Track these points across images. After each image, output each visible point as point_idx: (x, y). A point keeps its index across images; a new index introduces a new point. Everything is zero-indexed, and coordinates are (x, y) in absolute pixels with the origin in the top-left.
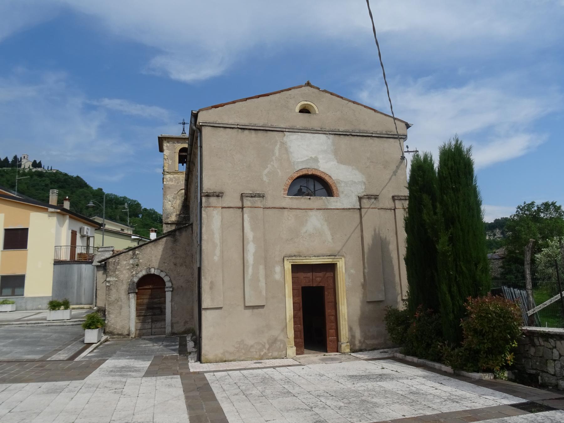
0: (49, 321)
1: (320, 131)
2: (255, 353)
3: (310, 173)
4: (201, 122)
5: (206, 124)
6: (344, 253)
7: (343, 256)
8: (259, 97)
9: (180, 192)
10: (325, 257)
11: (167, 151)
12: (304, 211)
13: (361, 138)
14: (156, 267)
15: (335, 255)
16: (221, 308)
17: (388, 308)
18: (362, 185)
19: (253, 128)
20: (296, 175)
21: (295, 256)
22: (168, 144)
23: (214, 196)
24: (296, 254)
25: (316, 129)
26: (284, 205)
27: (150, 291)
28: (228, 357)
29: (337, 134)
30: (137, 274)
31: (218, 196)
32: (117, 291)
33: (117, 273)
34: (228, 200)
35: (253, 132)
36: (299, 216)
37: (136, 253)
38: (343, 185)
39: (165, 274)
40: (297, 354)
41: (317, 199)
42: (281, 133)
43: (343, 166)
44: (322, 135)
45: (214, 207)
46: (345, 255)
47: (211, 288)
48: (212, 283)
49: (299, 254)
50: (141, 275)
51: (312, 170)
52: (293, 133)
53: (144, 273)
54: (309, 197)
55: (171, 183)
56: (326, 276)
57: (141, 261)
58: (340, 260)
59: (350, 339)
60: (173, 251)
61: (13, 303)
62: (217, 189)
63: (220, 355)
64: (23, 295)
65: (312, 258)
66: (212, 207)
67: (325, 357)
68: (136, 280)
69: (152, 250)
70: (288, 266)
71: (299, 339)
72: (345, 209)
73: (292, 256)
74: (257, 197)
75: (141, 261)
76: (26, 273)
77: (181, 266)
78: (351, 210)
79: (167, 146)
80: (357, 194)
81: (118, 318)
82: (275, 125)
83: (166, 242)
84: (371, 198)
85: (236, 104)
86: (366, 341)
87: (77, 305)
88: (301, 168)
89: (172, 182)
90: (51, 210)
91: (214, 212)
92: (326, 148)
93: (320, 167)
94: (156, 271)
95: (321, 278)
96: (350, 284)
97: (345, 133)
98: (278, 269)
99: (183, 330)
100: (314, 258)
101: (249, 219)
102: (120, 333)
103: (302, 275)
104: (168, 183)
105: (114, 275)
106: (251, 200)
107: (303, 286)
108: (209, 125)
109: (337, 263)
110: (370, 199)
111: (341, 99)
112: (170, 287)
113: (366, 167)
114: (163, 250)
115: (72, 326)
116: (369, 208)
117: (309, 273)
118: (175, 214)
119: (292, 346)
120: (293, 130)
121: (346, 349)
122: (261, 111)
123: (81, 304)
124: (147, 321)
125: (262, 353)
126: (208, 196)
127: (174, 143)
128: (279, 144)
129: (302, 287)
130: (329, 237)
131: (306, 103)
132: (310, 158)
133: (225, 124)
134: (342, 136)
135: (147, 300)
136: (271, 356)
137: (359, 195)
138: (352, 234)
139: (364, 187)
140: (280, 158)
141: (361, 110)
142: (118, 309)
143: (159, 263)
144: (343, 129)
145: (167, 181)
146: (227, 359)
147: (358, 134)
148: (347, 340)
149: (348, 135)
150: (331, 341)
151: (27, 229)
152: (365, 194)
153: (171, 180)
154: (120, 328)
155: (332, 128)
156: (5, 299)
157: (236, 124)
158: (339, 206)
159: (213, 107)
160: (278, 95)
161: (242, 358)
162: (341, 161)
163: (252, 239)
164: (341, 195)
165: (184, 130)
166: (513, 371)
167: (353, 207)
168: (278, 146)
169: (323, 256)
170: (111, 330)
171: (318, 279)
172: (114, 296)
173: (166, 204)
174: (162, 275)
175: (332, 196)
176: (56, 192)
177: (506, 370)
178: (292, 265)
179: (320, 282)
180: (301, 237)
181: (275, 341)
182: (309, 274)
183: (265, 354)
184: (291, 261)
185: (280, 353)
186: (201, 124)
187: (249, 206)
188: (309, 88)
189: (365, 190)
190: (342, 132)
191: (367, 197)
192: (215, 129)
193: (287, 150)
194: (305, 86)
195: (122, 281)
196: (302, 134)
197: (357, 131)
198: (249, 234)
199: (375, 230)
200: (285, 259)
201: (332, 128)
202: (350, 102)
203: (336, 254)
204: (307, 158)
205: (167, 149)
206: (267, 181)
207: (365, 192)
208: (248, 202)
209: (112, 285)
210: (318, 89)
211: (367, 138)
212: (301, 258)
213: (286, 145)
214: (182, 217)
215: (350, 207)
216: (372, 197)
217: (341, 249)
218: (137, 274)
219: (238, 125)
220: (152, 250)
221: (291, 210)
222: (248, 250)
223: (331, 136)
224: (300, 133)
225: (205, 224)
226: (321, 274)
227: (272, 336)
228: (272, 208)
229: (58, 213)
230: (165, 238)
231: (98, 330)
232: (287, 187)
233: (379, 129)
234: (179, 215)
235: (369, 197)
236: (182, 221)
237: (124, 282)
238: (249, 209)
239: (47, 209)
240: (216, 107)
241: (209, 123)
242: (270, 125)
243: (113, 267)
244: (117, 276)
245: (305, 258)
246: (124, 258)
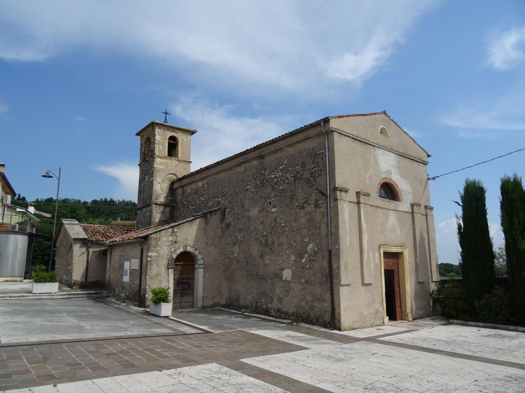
0: (35, 294)
9: (167, 176)
10: (397, 247)
11: (159, 136)
14: (191, 245)
16: (349, 285)
22: (160, 130)
26: (377, 204)
27: (180, 267)
30: (175, 250)
32: (158, 266)
33: (158, 248)
37: (175, 231)
39: (199, 252)
43: (402, 179)
47: (346, 268)
48: (346, 263)
50: (179, 252)
53: (181, 250)
55: (160, 167)
57: (179, 238)
60: (205, 231)
68: (175, 256)
69: (188, 229)
75: (179, 238)
77: (211, 245)
79: (158, 132)
83: (200, 222)
85: (350, 117)
86: (418, 312)
87: (11, 277)
89: (162, 166)
94: (191, 248)
97: (403, 155)
99: (211, 303)
100: (393, 247)
104: (158, 166)
105: (155, 250)
109: (403, 253)
112: (203, 264)
114: (197, 230)
115: (63, 300)
118: (163, 196)
123: (15, 277)
124: (177, 295)
127: (164, 130)
128: (373, 155)
135: (178, 275)
143: (194, 242)
145: (157, 164)
153: (161, 164)
161: (362, 326)
165: (166, 119)
168: (372, 157)
172: (154, 270)
173: (156, 186)
174: (197, 253)
175: (395, 200)
186: (333, 129)
192: (341, 135)
195: (162, 256)
205: (159, 135)
209: (153, 259)
210: (389, 117)
212: (387, 247)
214: (169, 199)
218: (175, 250)
219: (353, 135)
220: (188, 229)
224: (382, 150)
230: (199, 219)
233: (415, 155)
234: (167, 197)
236: (169, 203)
237: (164, 257)
240: (340, 117)
244: (157, 252)
246: (165, 234)
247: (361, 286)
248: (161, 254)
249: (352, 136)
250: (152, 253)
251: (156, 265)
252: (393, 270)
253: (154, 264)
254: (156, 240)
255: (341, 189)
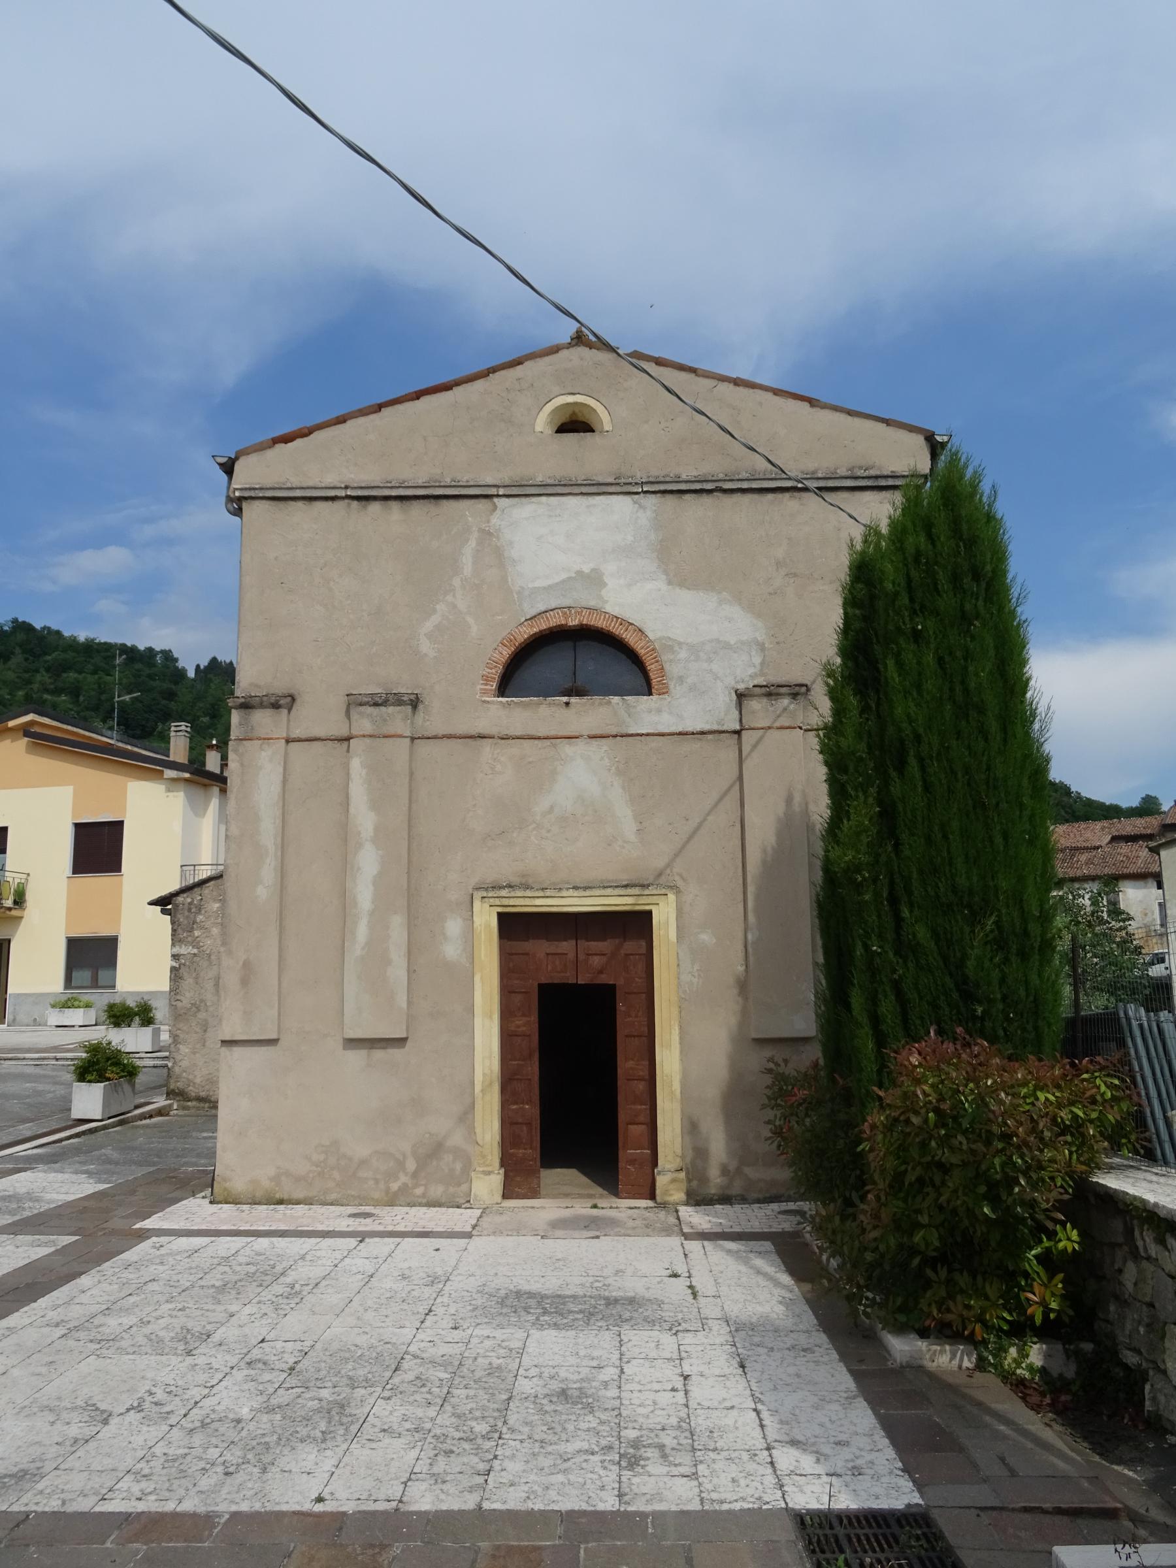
1: (612, 484)
2: (371, 1182)
3: (573, 622)
4: (237, 489)
5: (252, 494)
6: (677, 878)
7: (671, 887)
8: (418, 395)
10: (609, 891)
12: (548, 742)
13: (756, 496)
15: (645, 883)
17: (777, 1065)
18: (753, 653)
19: (394, 493)
20: (525, 632)
21: (510, 886)
23: (265, 707)
24: (515, 880)
25: (601, 479)
26: (481, 726)
28: (287, 1189)
29: (671, 492)
31: (276, 706)
33: (196, 933)
34: (305, 721)
35: (395, 505)
36: (531, 759)
38: (683, 654)
40: (505, 1196)
41: (593, 704)
42: (483, 501)
43: (686, 595)
44: (621, 497)
45: (265, 739)
46: (680, 883)
47: (245, 982)
48: (247, 965)
49: (524, 881)
51: (580, 613)
52: (523, 500)
54: (565, 699)
56: (622, 952)
58: (661, 901)
59: (688, 1160)
61: (88, 1006)
62: (279, 687)
63: (266, 1184)
64: (114, 987)
65: (564, 893)
66: (259, 739)
67: (595, 1212)
70: (486, 919)
71: (525, 1149)
72: (686, 734)
73: (501, 888)
74: (393, 704)
76: (121, 932)
78: (710, 737)
80: (733, 683)
81: (197, 1055)
82: (465, 479)
84: (778, 694)
85: (350, 423)
86: (748, 1170)
88: (543, 609)
90: (170, 773)
91: (263, 754)
92: (630, 538)
93: (607, 602)
95: (604, 959)
96: (695, 980)
97: (698, 486)
98: (454, 927)
100: (571, 893)
101: (364, 772)
102: (203, 1094)
103: (540, 948)
105: (190, 939)
106: (375, 714)
107: (544, 981)
108: (261, 495)
110: (773, 697)
111: (693, 375)
113: (770, 594)
116: (769, 728)
117: (565, 940)
119: (490, 1169)
120: (521, 491)
121: (672, 1192)
122: (425, 439)
125: (395, 1186)
126: (246, 706)
129: (541, 986)
130: (628, 827)
131: (570, 399)
132: (574, 575)
133: (308, 488)
134: (687, 497)
136: (424, 1195)
137: (739, 687)
138: (708, 814)
139: (757, 660)
140: (476, 582)
141: (761, 404)
142: (198, 1030)
144: (695, 473)
146: (286, 1197)
147: (745, 485)
148: (678, 1163)
149: (710, 492)
150: (632, 1162)
151: (121, 823)
152: (760, 681)
154: (203, 1084)
155: (656, 472)
156: (70, 996)
157: (343, 486)
158: (667, 723)
159: (276, 441)
160: (479, 385)
161: (333, 1196)
162: (680, 580)
163: (372, 834)
164: (676, 690)
166: (1072, 1347)
167: (715, 727)
169: (605, 887)
170: (180, 1085)
171: (596, 961)
172: (188, 995)
176: (183, 728)
177: (1035, 1339)
178: (500, 915)
179: (601, 972)
180: (534, 825)
181: (437, 1149)
182: (565, 943)
183: (404, 1189)
184: (497, 902)
185: (451, 1190)
186: (237, 494)
187: (366, 733)
188: (582, 351)
189: (761, 670)
190: (686, 482)
191: (763, 690)
192: (281, 504)
193: (499, 553)
194: (569, 346)
195: (209, 955)
196: (552, 499)
197: (744, 475)
198: (364, 819)
199: (789, 800)
200: (478, 895)
201: (656, 474)
202: (723, 381)
203: (651, 880)
204: (564, 576)
206: (432, 654)
207: (762, 674)
208: (364, 722)
209: (184, 965)
211: (779, 496)
212: (529, 893)
213: (498, 538)
215: (707, 727)
216: (783, 690)
217: (668, 865)
219: (346, 487)
221: (503, 741)
222: (359, 869)
223: (652, 500)
224: (544, 499)
225: (235, 790)
226: (605, 946)
227: (427, 1136)
228: (444, 737)
229: (186, 780)
231: (105, 1086)
232: (494, 671)
235: (771, 692)
237: (213, 957)
238: (367, 740)
239: (163, 771)
240: (286, 439)
241: (261, 489)
242: (448, 480)
243: (187, 917)
244: (195, 943)
245: (541, 894)
246: (215, 893)
247: (341, 1047)
248: (205, 948)
249: (342, 493)
250: (181, 947)
251: (191, 980)
252: (611, 989)
253: (185, 974)
254: (189, 910)
255: (243, 700)
